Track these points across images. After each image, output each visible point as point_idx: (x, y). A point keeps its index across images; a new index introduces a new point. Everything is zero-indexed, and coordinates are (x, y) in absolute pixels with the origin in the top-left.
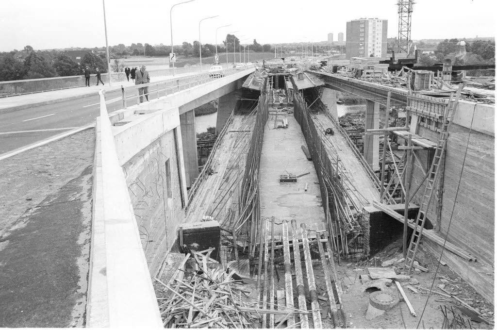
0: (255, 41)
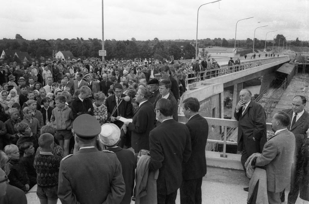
0: (297, 38)
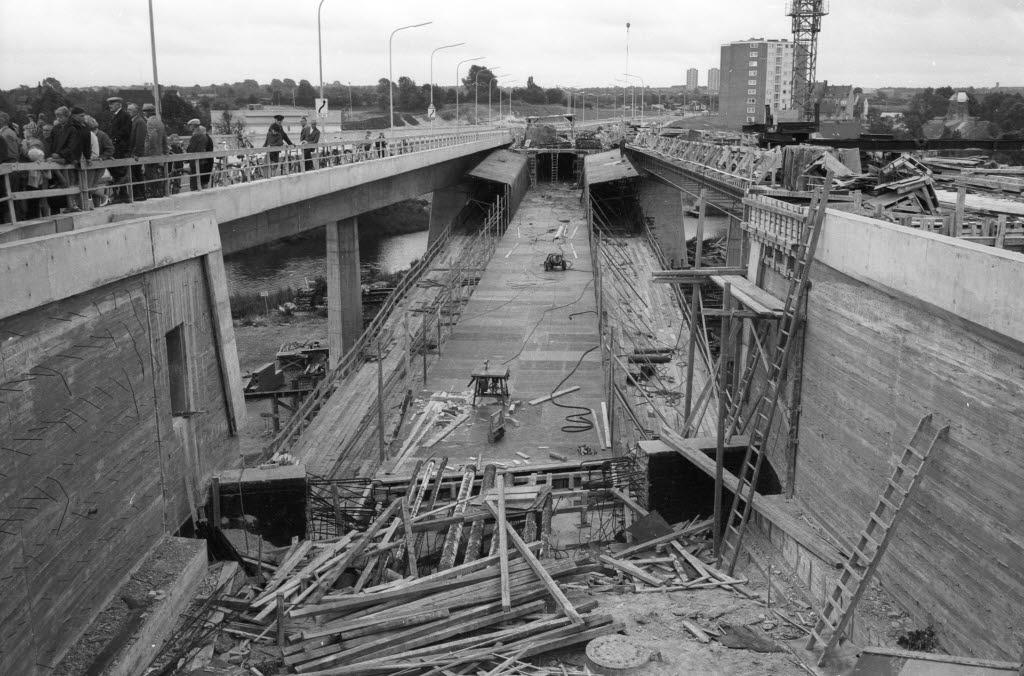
0: (530, 80)
